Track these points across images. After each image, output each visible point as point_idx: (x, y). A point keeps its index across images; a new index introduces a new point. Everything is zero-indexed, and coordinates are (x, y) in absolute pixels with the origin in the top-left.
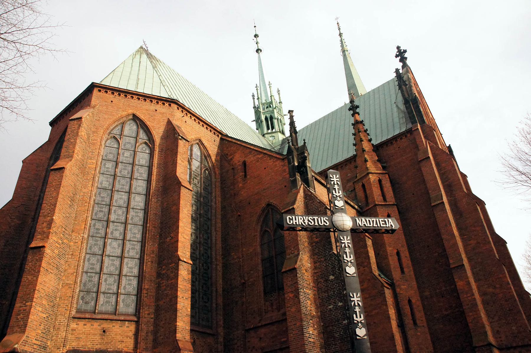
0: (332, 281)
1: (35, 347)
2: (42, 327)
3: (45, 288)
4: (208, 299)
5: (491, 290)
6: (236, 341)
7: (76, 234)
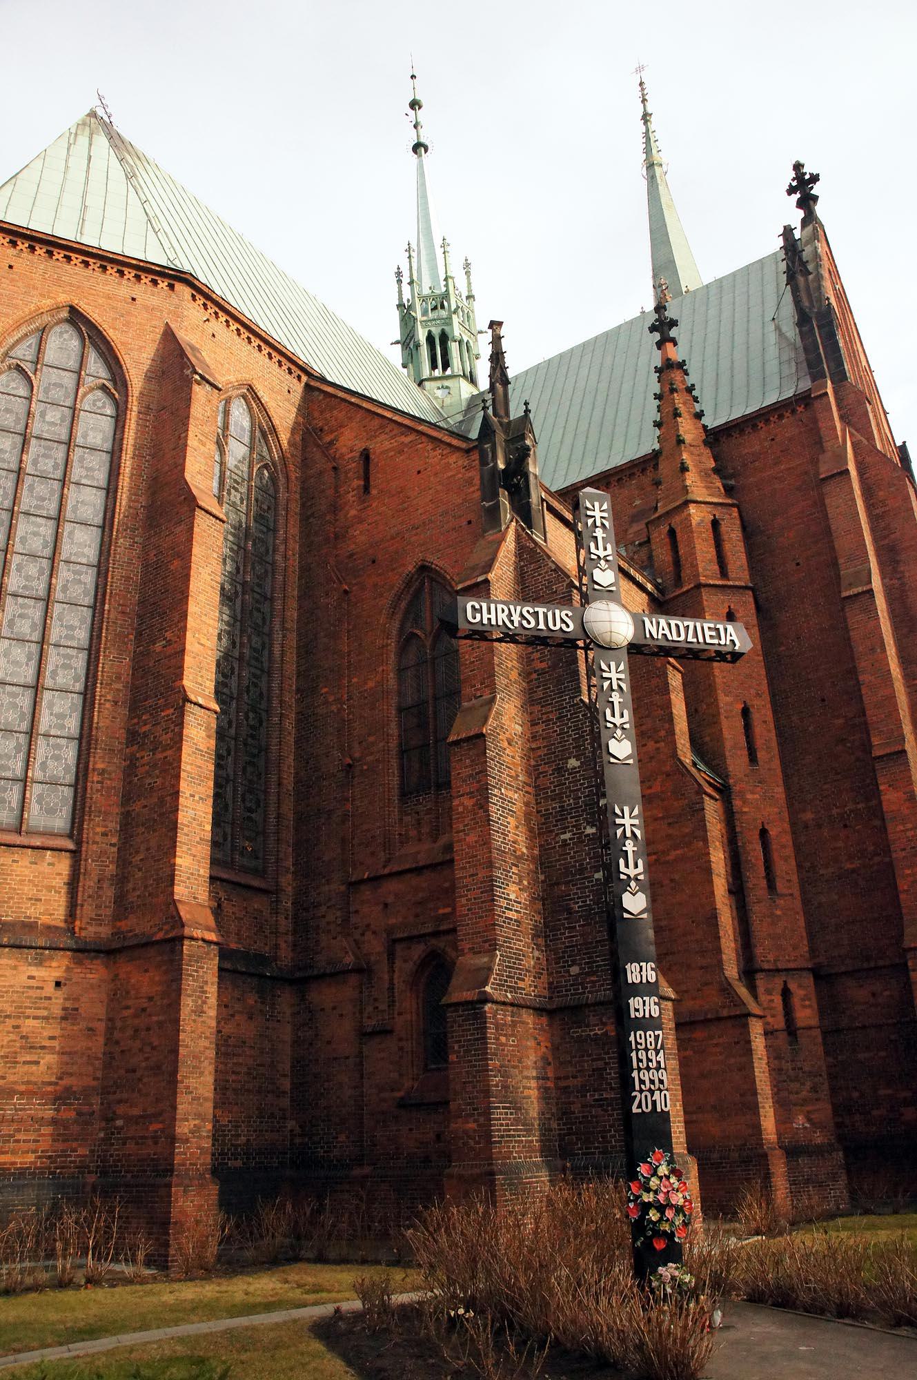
0: (573, 771)
4: (258, 803)
6: (323, 909)
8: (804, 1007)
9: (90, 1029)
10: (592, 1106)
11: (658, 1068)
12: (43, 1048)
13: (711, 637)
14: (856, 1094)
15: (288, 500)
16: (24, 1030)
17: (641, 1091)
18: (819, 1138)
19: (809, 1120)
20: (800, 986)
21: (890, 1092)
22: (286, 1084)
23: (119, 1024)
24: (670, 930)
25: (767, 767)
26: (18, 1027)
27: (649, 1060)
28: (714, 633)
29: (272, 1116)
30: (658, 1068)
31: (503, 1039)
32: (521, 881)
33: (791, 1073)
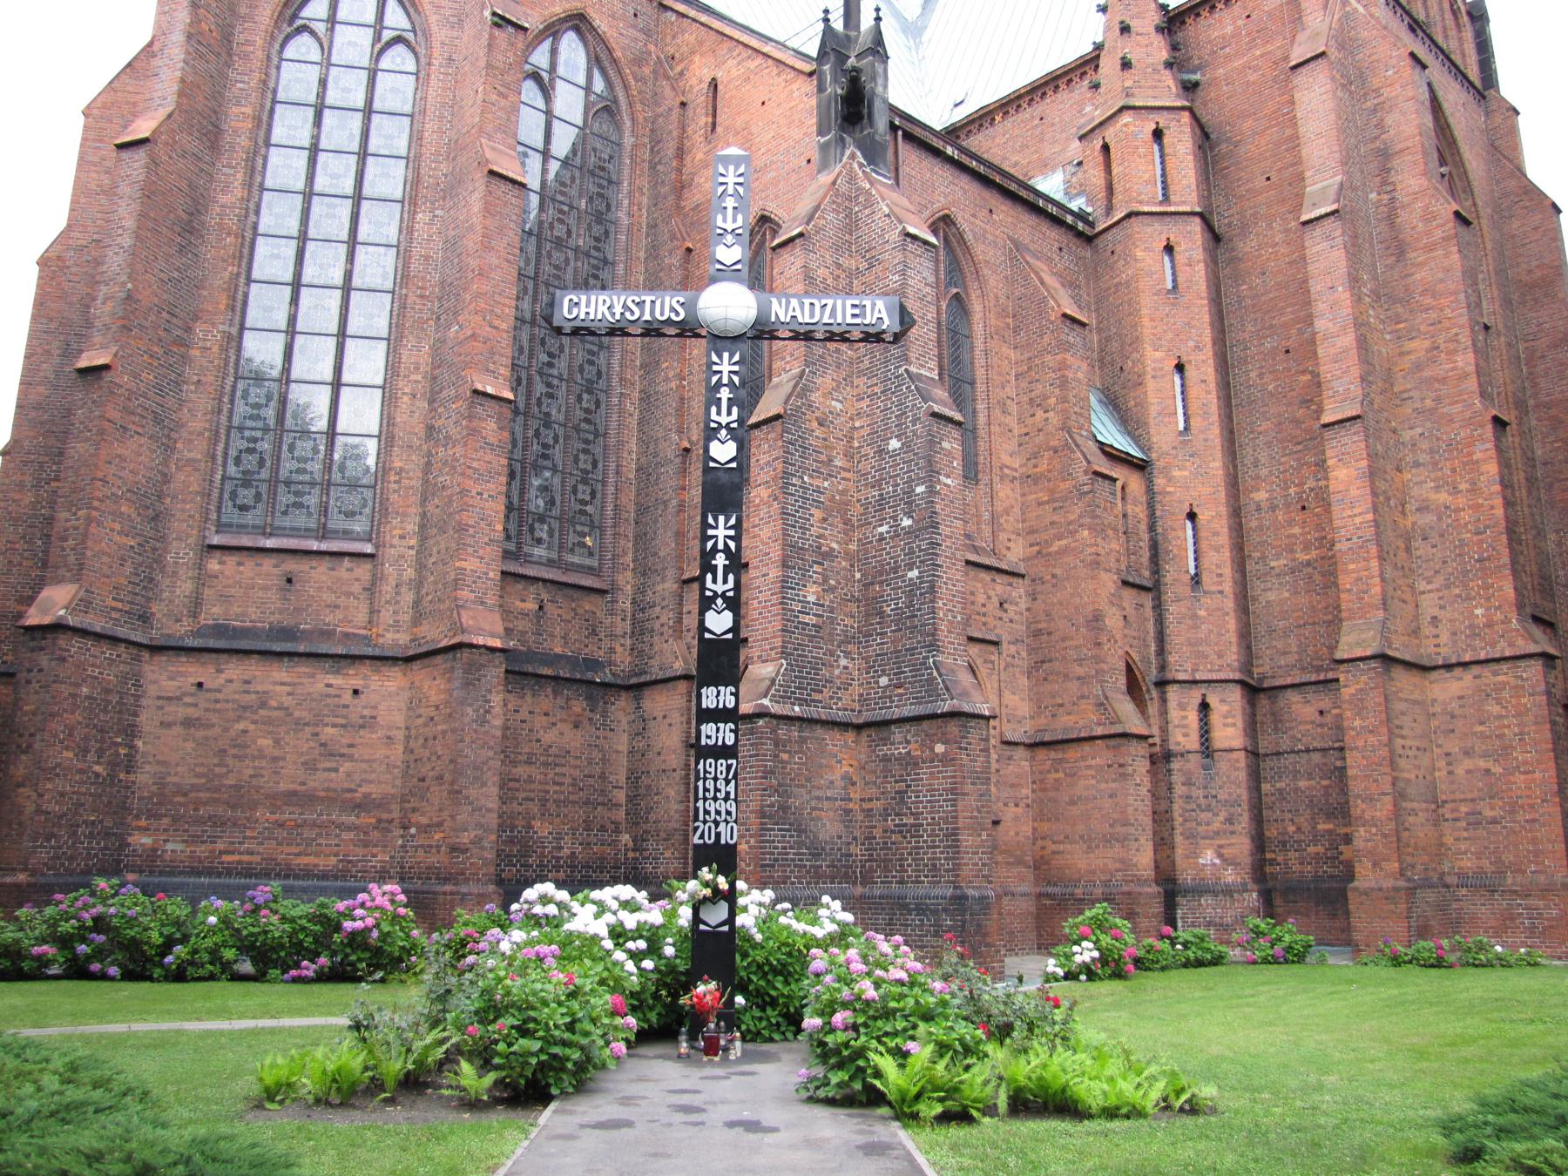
0: (895, 454)
1: (114, 615)
2: (128, 569)
3: (126, 474)
4: (593, 494)
5: (1443, 497)
6: (658, 609)
7: (204, 327)
8: (1225, 725)
9: (389, 738)
10: (893, 832)
11: (726, 799)
12: (342, 755)
13: (854, 316)
14: (1291, 829)
15: (635, 146)
16: (323, 738)
17: (705, 822)
18: (1230, 876)
19: (1220, 856)
20: (1222, 701)
21: (1331, 826)
22: (621, 796)
23: (413, 732)
24: (1050, 634)
25: (1202, 437)
26: (317, 734)
27: (717, 790)
28: (857, 311)
29: (603, 828)
30: (726, 799)
31: (785, 756)
32: (825, 581)
33: (1202, 801)
